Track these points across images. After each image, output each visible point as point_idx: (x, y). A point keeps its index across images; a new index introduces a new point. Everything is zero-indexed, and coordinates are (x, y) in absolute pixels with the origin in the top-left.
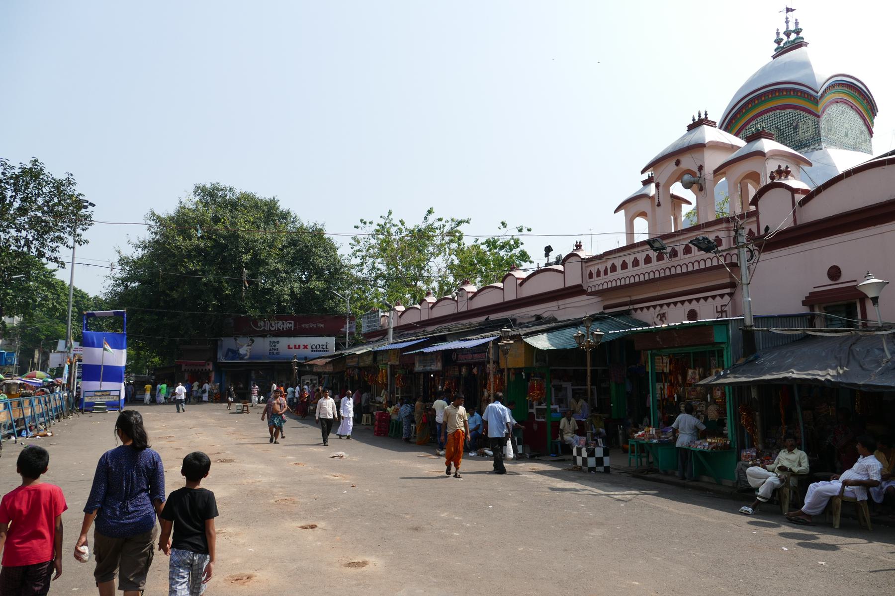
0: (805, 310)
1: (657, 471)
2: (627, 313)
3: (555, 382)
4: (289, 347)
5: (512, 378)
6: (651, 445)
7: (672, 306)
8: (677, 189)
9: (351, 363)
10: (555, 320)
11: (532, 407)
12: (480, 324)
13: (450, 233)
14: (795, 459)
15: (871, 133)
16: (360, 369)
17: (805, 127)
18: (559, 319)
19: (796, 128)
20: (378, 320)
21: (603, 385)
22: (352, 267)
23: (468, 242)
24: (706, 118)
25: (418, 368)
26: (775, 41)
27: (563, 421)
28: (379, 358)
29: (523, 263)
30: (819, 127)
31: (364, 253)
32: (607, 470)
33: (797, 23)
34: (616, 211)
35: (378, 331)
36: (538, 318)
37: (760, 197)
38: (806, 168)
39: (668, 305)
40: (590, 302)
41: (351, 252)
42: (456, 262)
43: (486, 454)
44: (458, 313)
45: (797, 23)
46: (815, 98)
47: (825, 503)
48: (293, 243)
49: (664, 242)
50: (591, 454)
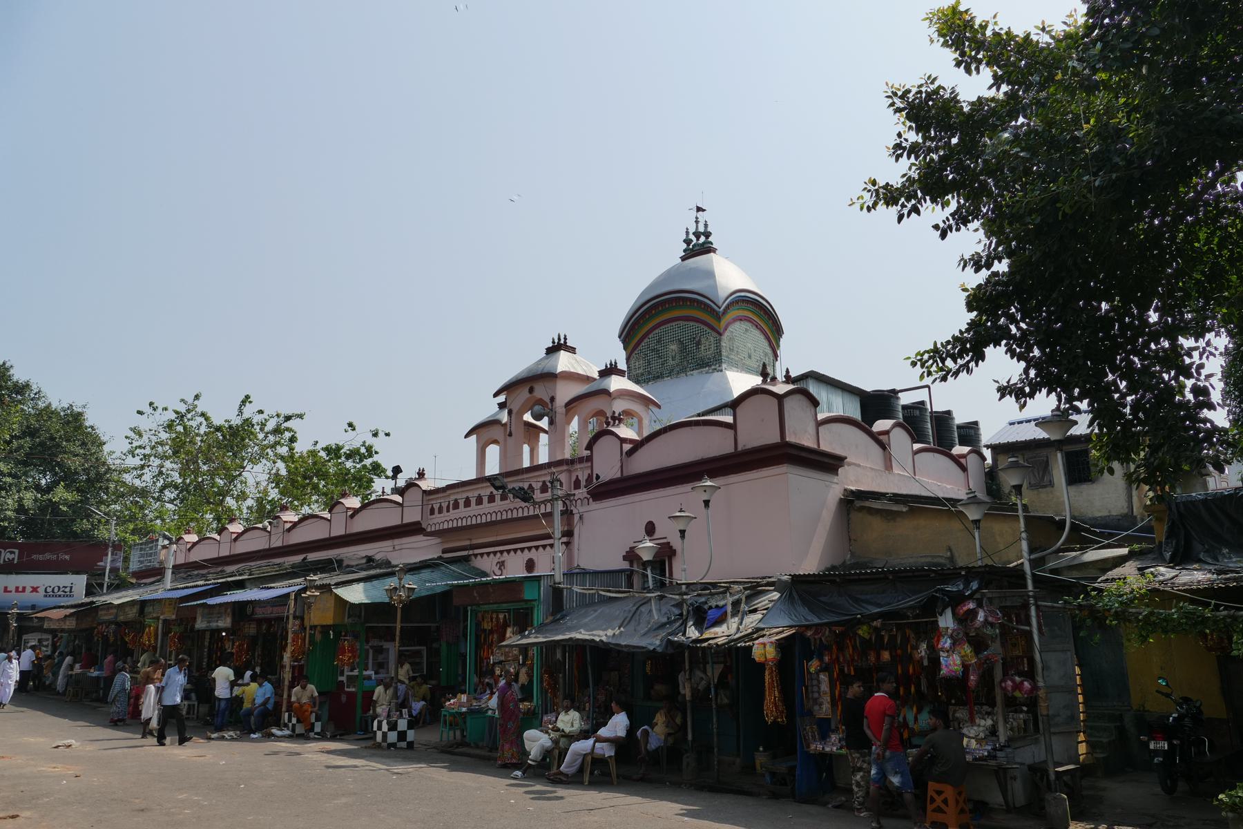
0: (625, 565)
1: (468, 745)
2: (466, 559)
3: (375, 642)
4: (6, 590)
5: (318, 637)
6: (462, 714)
8: (528, 417)
9: (105, 616)
10: (388, 563)
11: (342, 674)
12: (293, 566)
13: (277, 431)
14: (569, 720)
15: (776, 356)
16: (118, 624)
18: (394, 563)
19: (699, 343)
20: (156, 553)
21: (434, 645)
22: (126, 471)
23: (302, 447)
25: (200, 624)
27: (379, 690)
28: (148, 609)
29: (376, 478)
31: (148, 451)
32: (411, 745)
33: (706, 225)
35: (154, 569)
36: (370, 559)
38: (655, 409)
39: (508, 551)
40: (426, 544)
41: (126, 447)
42: (283, 472)
43: (273, 735)
44: (270, 549)
45: (706, 225)
46: (717, 313)
47: (580, 760)
48: (30, 432)
49: (506, 480)
50: (393, 727)
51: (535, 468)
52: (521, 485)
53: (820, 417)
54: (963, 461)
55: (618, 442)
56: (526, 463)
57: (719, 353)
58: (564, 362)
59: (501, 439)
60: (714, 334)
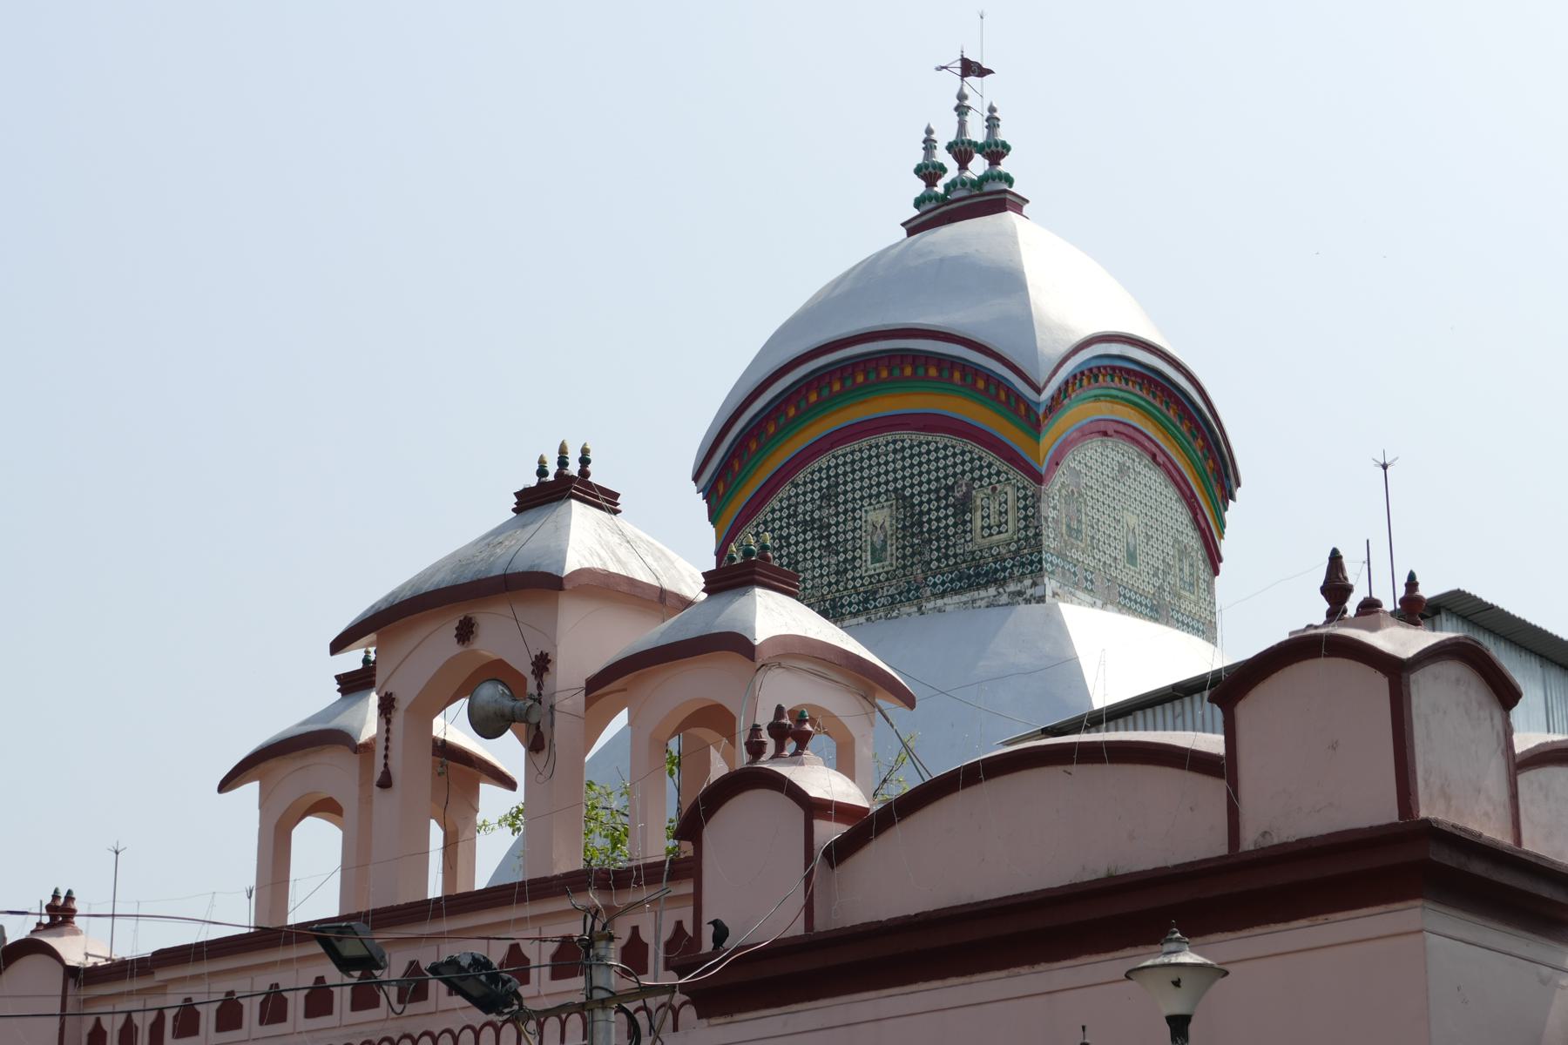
8: (453, 726)
15: (1214, 559)
17: (994, 507)
19: (964, 507)
24: (584, 473)
26: (919, 171)
30: (1037, 515)
33: (992, 122)
34: (227, 784)
37: (710, 813)
45: (992, 122)
46: (1030, 407)
51: (460, 903)
52: (478, 948)
53: (1524, 741)
55: (799, 814)
56: (435, 890)
57: (1035, 541)
58: (585, 542)
59: (348, 798)
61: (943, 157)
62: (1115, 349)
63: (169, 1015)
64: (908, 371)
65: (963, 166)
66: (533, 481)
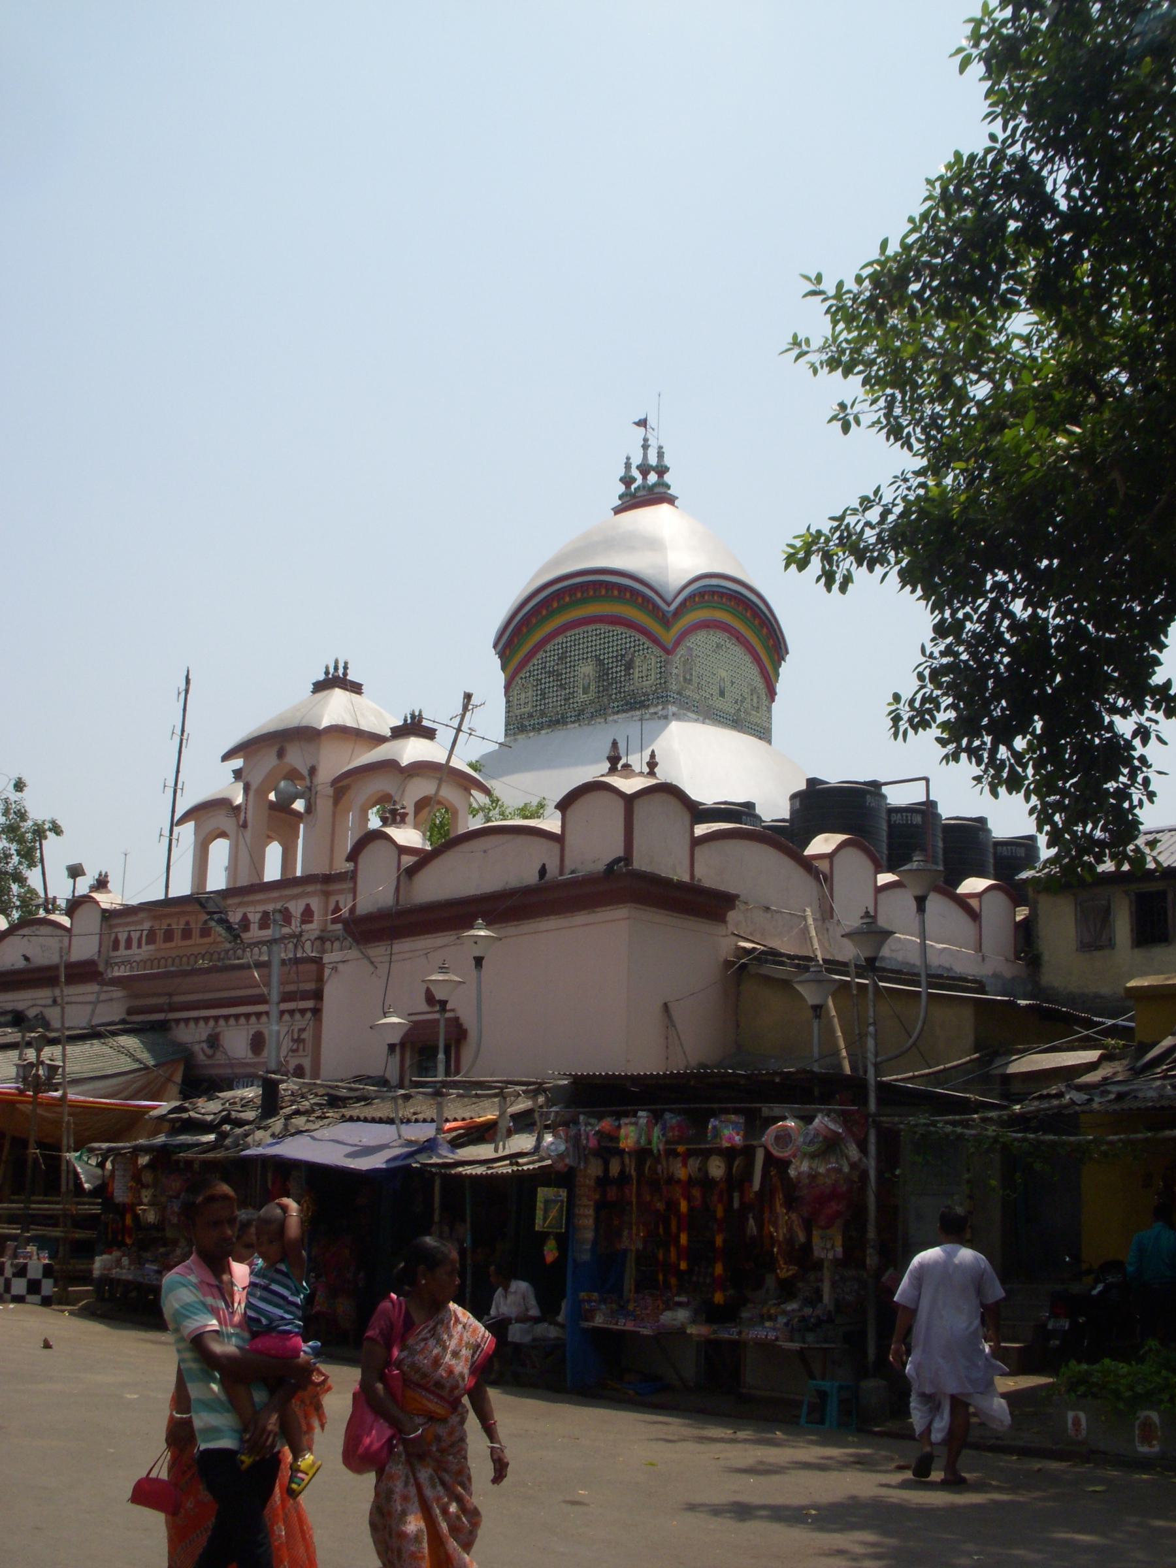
7: (232, 1021)
15: (772, 693)
19: (629, 666)
24: (345, 674)
26: (621, 480)
33: (661, 455)
45: (661, 455)
54: (974, 903)
55: (395, 852)
60: (657, 651)
61: (636, 473)
62: (714, 582)
63: (145, 933)
64: (603, 592)
65: (645, 477)
66: (322, 677)
